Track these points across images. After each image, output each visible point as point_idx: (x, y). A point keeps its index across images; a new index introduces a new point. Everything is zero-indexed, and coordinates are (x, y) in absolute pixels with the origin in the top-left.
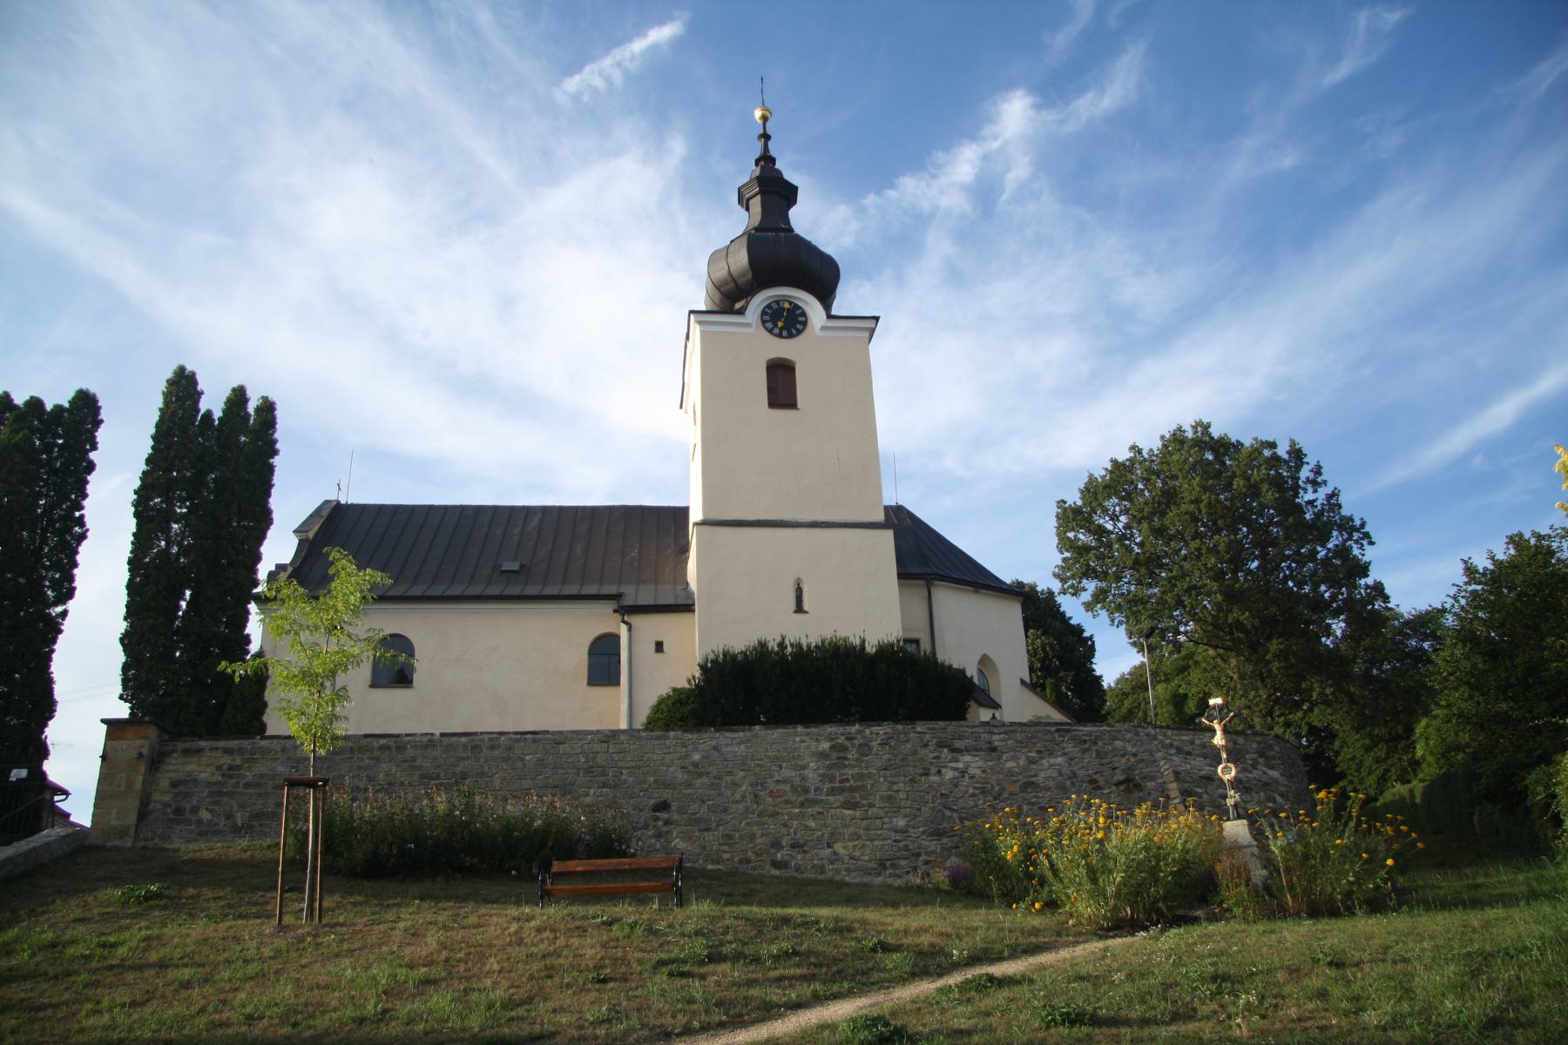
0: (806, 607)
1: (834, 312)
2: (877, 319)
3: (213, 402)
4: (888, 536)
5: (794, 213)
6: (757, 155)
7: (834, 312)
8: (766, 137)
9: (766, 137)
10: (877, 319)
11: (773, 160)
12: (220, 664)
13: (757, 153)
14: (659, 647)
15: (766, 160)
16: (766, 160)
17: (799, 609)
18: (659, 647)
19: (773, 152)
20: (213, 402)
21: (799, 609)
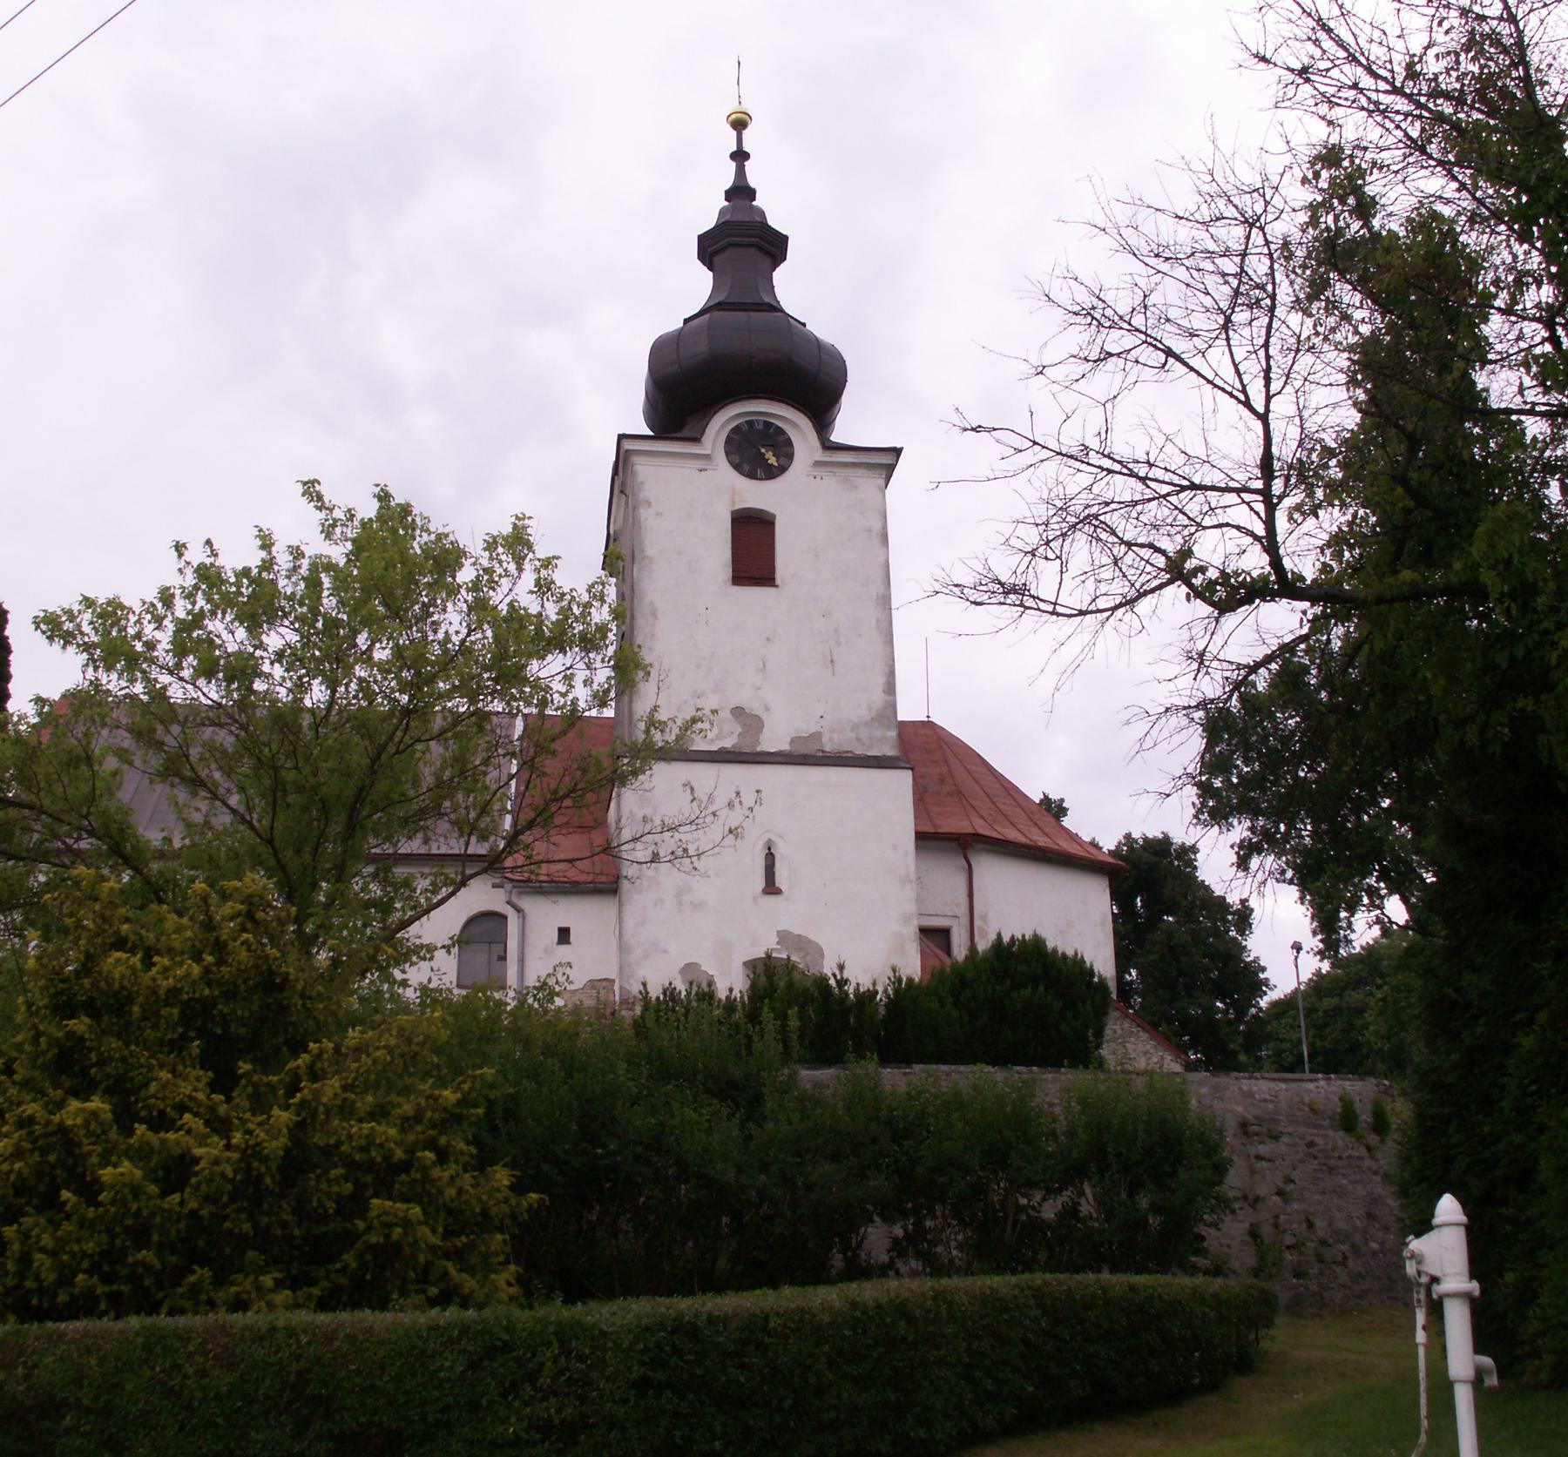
0: (781, 880)
1: (837, 436)
2: (897, 452)
3: (1006, 939)
4: (901, 782)
5: (780, 276)
6: (728, 184)
7: (837, 436)
8: (740, 156)
9: (740, 156)
10: (897, 452)
11: (751, 194)
12: (1502, 422)
13: (728, 181)
14: (564, 935)
15: (741, 192)
16: (741, 192)
17: (771, 888)
18: (564, 935)
19: (752, 180)
20: (1006, 939)
21: (771, 888)
